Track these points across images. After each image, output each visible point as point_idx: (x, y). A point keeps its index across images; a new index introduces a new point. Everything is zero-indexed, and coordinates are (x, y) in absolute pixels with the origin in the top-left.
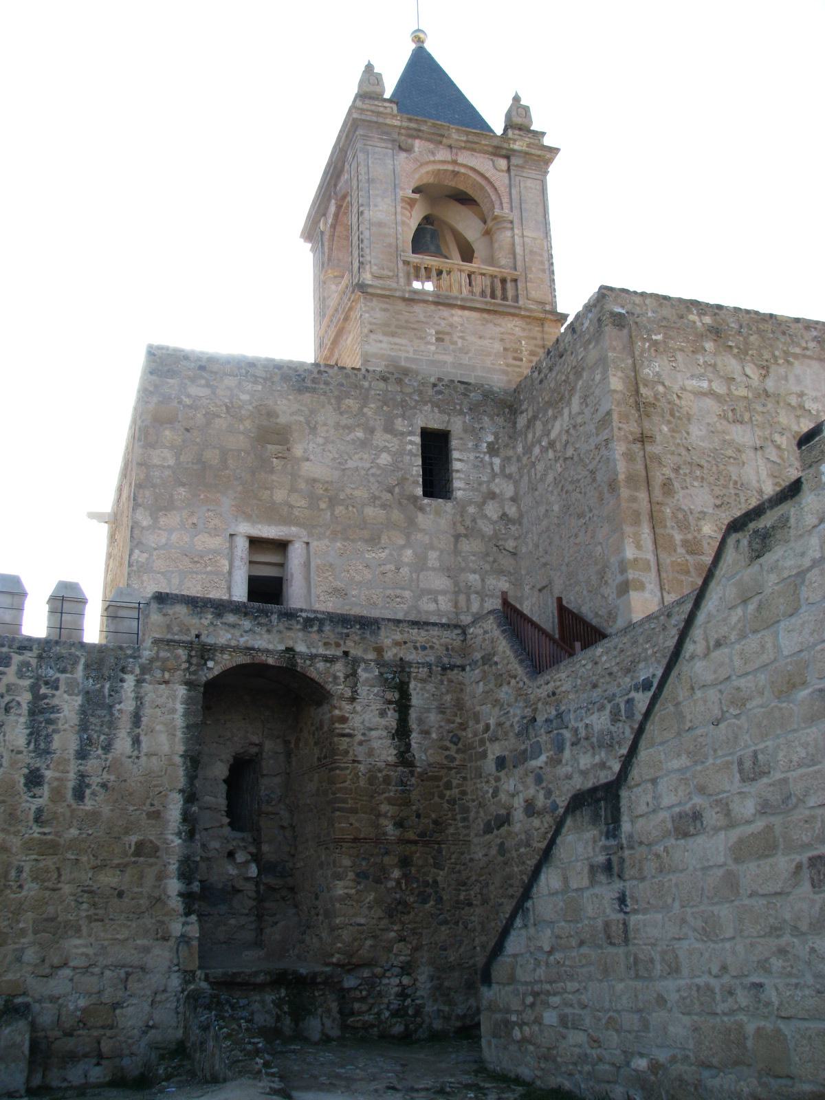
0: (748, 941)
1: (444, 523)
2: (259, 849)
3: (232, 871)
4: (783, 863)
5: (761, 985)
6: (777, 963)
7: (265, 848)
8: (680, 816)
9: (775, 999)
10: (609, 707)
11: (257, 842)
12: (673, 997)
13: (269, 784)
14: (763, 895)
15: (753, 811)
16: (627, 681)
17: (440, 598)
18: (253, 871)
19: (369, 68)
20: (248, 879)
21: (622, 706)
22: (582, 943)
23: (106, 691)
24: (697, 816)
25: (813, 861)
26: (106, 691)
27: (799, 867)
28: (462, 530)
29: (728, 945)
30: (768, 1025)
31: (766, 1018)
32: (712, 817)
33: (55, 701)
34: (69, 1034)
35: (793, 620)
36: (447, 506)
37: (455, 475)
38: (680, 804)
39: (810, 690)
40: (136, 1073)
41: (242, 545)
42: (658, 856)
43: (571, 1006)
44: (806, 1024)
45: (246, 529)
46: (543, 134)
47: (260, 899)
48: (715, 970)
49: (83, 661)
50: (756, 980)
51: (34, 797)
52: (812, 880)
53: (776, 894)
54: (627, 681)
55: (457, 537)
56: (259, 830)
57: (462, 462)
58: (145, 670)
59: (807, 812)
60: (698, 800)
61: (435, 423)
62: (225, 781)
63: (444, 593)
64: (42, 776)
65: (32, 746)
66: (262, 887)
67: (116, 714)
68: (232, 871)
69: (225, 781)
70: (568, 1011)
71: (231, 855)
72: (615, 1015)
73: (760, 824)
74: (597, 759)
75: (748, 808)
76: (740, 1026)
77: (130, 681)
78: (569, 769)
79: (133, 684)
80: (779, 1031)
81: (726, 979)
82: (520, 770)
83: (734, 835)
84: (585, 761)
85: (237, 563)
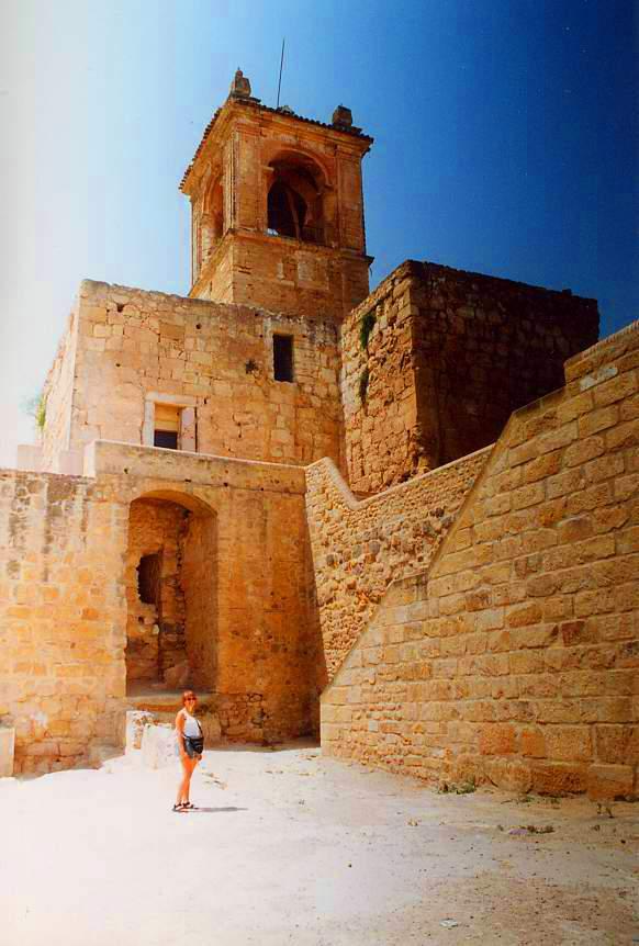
0: (518, 676)
1: (289, 398)
2: (160, 615)
3: (143, 630)
4: (543, 628)
5: (527, 703)
6: (538, 690)
7: (164, 614)
8: (472, 596)
9: (536, 713)
10: (412, 526)
11: (158, 610)
12: (464, 711)
13: (167, 569)
14: (530, 648)
15: (524, 594)
16: (425, 510)
17: (285, 448)
18: (156, 630)
19: (239, 74)
20: (152, 636)
21: (421, 525)
22: (398, 678)
23: (63, 507)
24: (484, 597)
25: (566, 627)
26: (63, 507)
27: (555, 632)
28: (301, 404)
29: (504, 678)
30: (531, 728)
31: (528, 723)
32: (495, 598)
33: (27, 514)
34: (38, 741)
35: (557, 476)
36: (291, 386)
37: (296, 365)
38: (472, 589)
39: (567, 521)
40: (204, 752)
41: (150, 407)
42: (455, 622)
43: (390, 718)
44: (557, 726)
45: (152, 396)
46: (361, 130)
47: (161, 652)
48: (495, 694)
49: (47, 485)
50: (524, 700)
51: (13, 578)
52: (564, 638)
53: (538, 647)
54: (425, 510)
55: (297, 407)
56: (160, 602)
57: (298, 355)
58: (90, 492)
59: (562, 596)
60: (485, 588)
61: (283, 331)
62: (137, 569)
63: (287, 445)
64: (18, 565)
65: (11, 544)
66: (162, 641)
67: (70, 523)
68: (143, 630)
69: (137, 569)
70: (386, 721)
71: (141, 619)
72: (422, 723)
73: (529, 603)
74: (402, 559)
75: (522, 592)
76: (512, 729)
77: (79, 499)
78: (381, 565)
79: (82, 501)
80: (538, 731)
81: (502, 699)
82: (345, 565)
83: (510, 610)
84: (393, 560)
85: (147, 420)
